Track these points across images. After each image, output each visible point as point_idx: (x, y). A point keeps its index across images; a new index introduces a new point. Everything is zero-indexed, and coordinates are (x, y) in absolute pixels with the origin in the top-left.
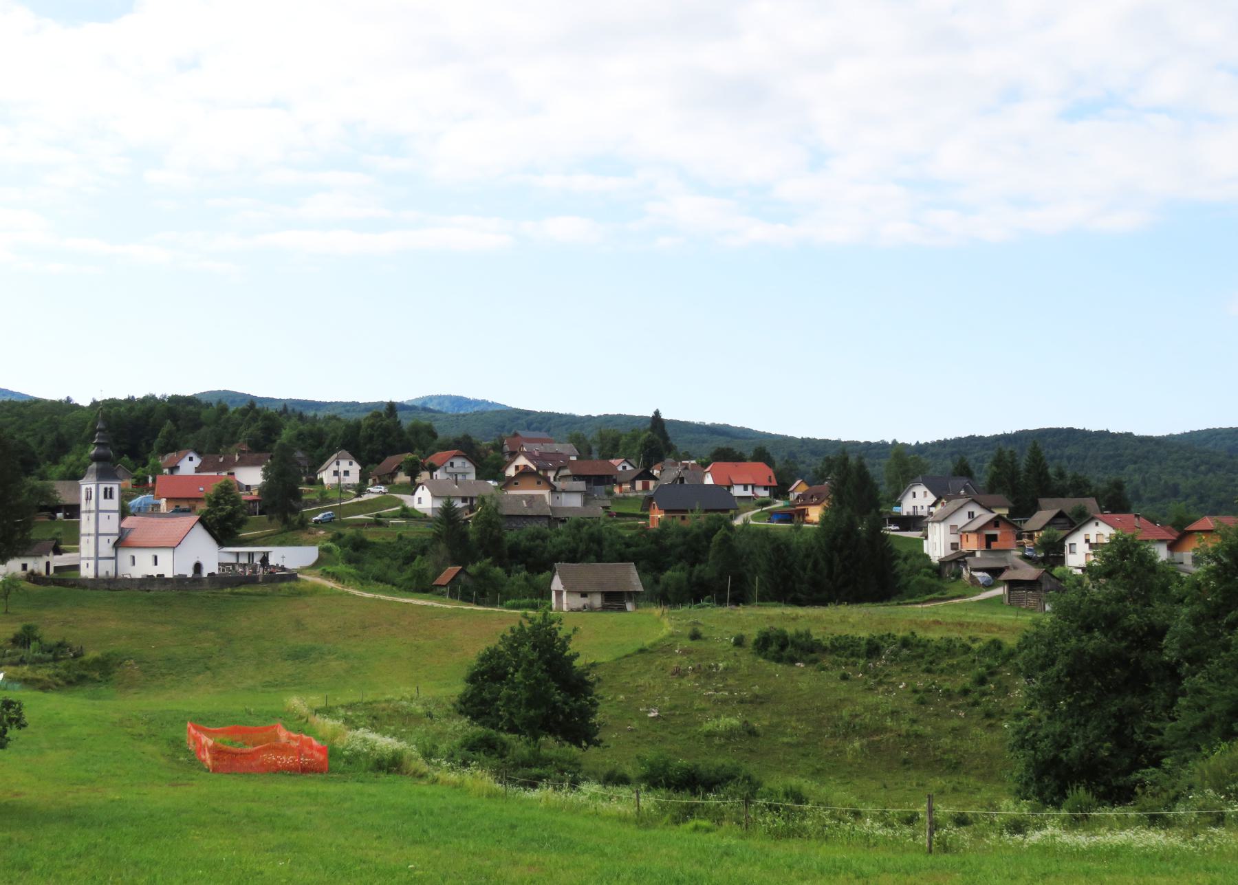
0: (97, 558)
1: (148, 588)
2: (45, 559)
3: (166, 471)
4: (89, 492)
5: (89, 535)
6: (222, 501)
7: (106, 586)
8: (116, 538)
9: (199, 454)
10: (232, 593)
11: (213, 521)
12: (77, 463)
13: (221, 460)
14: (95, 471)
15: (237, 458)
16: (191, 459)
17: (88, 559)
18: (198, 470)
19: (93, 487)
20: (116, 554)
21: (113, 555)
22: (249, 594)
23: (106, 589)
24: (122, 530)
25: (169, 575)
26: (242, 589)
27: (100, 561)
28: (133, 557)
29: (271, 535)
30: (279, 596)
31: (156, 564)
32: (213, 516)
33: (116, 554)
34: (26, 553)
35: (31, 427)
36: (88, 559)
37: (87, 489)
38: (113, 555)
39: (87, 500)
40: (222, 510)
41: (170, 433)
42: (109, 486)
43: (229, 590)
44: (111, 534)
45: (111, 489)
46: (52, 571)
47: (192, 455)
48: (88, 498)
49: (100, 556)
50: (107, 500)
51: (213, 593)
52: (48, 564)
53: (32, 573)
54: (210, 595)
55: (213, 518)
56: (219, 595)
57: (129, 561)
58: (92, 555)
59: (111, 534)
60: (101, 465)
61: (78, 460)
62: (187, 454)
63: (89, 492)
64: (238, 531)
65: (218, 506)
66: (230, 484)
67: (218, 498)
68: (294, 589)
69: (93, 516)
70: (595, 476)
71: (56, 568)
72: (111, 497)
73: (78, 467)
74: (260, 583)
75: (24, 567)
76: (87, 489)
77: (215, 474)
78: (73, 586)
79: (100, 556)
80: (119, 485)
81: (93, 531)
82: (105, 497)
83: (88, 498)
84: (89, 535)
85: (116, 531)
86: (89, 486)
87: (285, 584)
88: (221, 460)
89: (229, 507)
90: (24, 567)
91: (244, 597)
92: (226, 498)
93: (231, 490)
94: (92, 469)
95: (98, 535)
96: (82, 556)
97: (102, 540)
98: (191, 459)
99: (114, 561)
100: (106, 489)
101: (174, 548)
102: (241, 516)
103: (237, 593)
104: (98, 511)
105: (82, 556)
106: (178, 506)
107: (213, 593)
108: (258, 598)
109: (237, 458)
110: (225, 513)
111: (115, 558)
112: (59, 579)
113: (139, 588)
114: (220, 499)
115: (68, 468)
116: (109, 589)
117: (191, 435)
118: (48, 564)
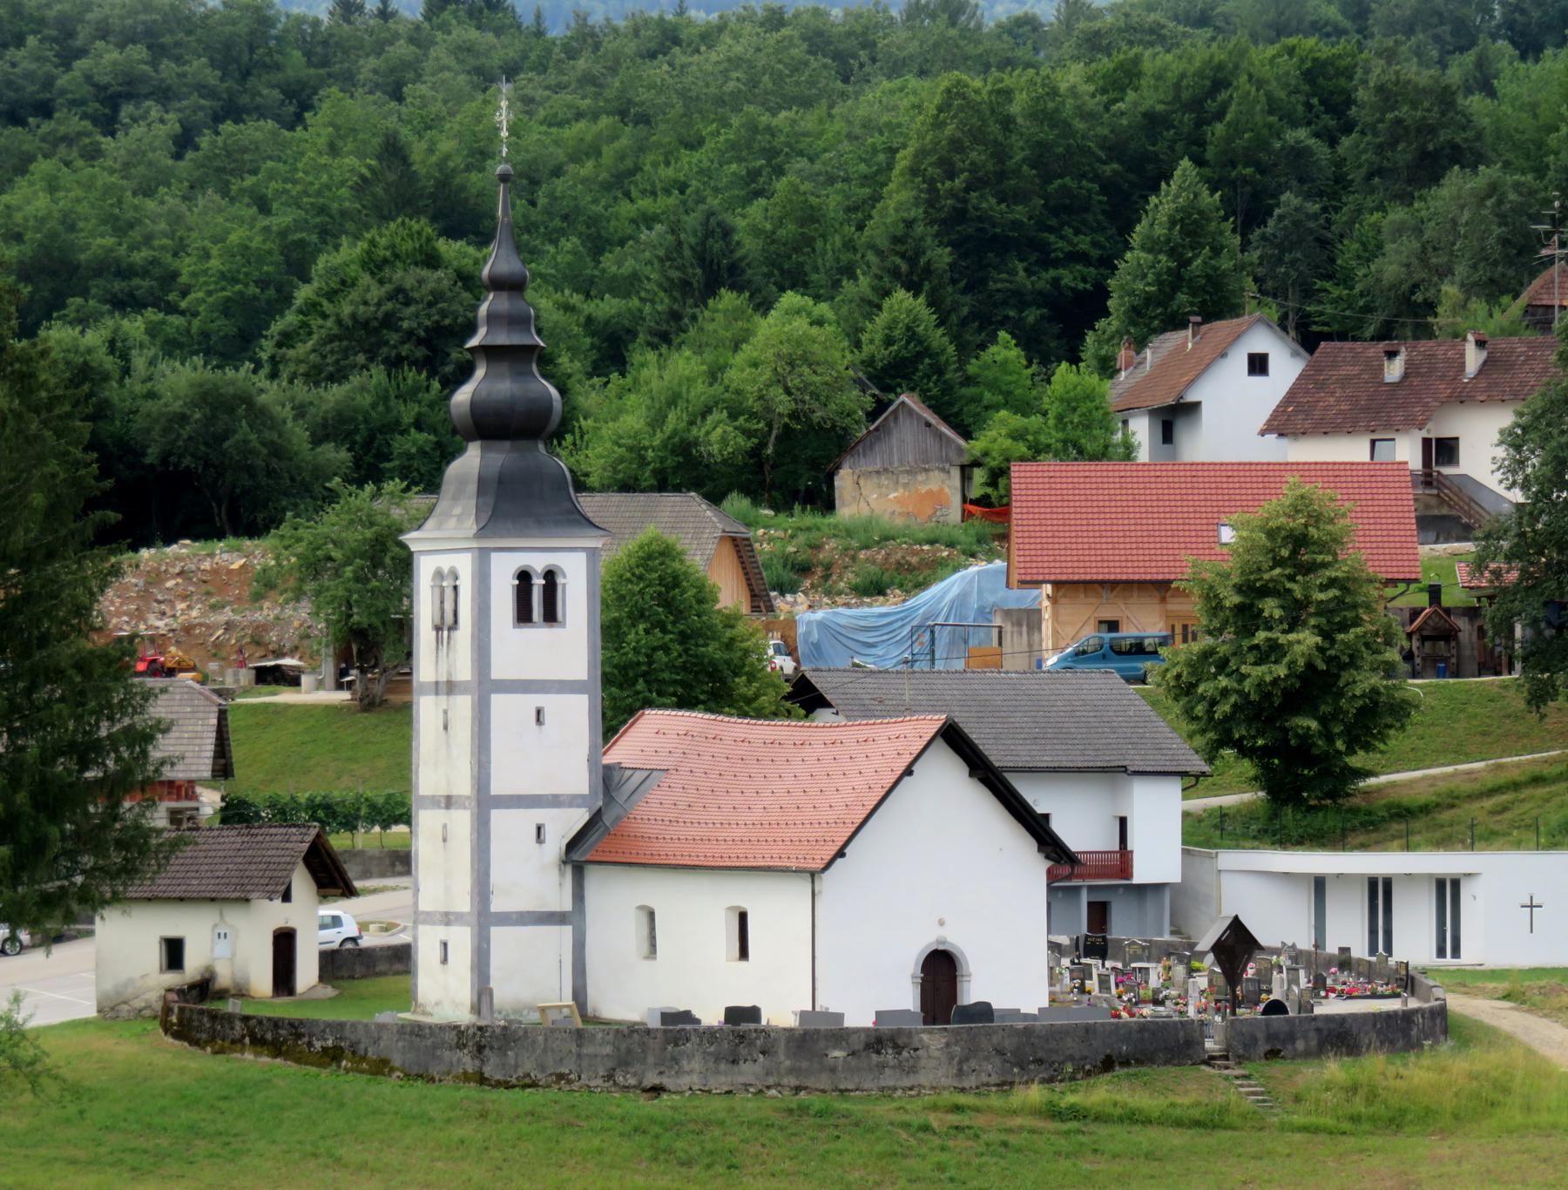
0: (484, 919)
1: (652, 1079)
2: (271, 915)
3: (1141, 430)
4: (447, 583)
5: (449, 802)
6: (1271, 607)
7: (468, 1062)
8: (578, 818)
9: (1308, 339)
10: (1054, 1113)
11: (1224, 708)
12: (700, 391)
13: (1394, 370)
14: (472, 488)
15: (1473, 359)
16: (1258, 365)
17: (448, 919)
18: (1283, 423)
19: (464, 564)
20: (579, 896)
21: (566, 904)
22: (1133, 1118)
23: (466, 1077)
24: (608, 780)
25: (781, 1013)
26: (1100, 1093)
27: (496, 933)
28: (743, 917)
29: (1537, 780)
30: (1284, 1128)
31: (744, 953)
32: (1223, 681)
33: (579, 896)
34: (133, 891)
35: (667, 173)
36: (448, 919)
37: (439, 575)
38: (566, 904)
39: (438, 629)
40: (1272, 652)
41: (1190, 226)
42: (538, 563)
43: (1035, 1094)
44: (555, 801)
45: (550, 575)
46: (307, 972)
47: (1262, 341)
48: (446, 626)
49: (497, 905)
50: (527, 632)
51: (957, 1109)
52: (284, 942)
53: (203, 988)
54: (933, 1120)
55: (1225, 692)
56: (980, 1121)
57: (631, 931)
58: (463, 903)
59: (555, 801)
60: (502, 456)
61: (714, 374)
62: (1237, 338)
63: (447, 583)
64: (1357, 760)
65: (1248, 631)
66: (1317, 518)
67: (1253, 590)
68: (1372, 1096)
69: (463, 705)
70: (760, 714)
71: (334, 964)
72: (551, 616)
73: (706, 412)
74: (1210, 1061)
75: (174, 952)
76: (439, 575)
77: (1354, 450)
78: (332, 1056)
79: (497, 905)
80: (592, 553)
81: (463, 786)
82: (523, 615)
83: (446, 626)
84: (449, 802)
85: (578, 780)
86: (445, 562)
87: (1334, 1069)
88: (1394, 370)
89: (1305, 641)
90: (174, 952)
91: (1103, 1131)
92: (1297, 590)
93: (1323, 547)
94: (462, 481)
95: (485, 802)
96: (424, 906)
97: (509, 827)
98: (1258, 365)
99: (567, 931)
100: (524, 577)
101: (813, 875)
102: (1366, 681)
103: (1076, 1113)
104: (485, 687)
105: (424, 906)
106: (1113, 626)
107: (957, 1109)
108: (1177, 1139)
109: (1473, 359)
110: (1281, 671)
111: (573, 917)
112: (276, 1024)
113: (610, 1077)
114: (1265, 592)
115: (657, 421)
116: (482, 1080)
117: (1398, 214)
118: (284, 942)
